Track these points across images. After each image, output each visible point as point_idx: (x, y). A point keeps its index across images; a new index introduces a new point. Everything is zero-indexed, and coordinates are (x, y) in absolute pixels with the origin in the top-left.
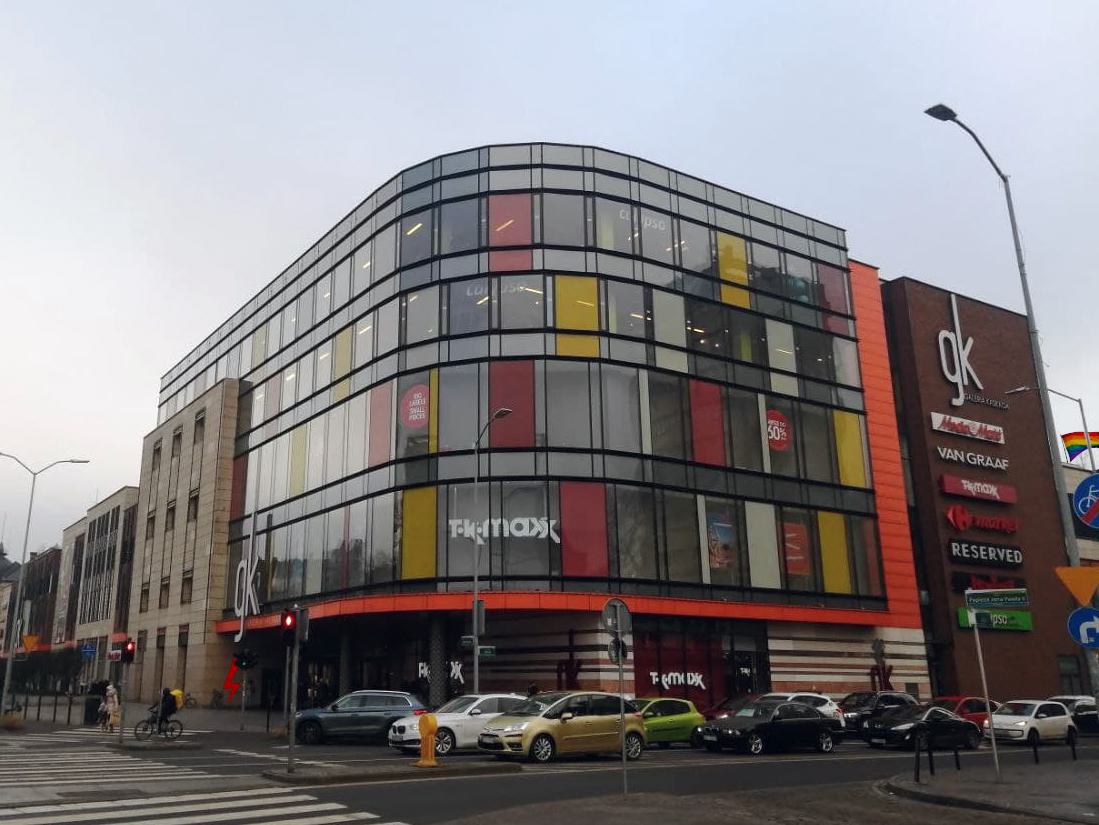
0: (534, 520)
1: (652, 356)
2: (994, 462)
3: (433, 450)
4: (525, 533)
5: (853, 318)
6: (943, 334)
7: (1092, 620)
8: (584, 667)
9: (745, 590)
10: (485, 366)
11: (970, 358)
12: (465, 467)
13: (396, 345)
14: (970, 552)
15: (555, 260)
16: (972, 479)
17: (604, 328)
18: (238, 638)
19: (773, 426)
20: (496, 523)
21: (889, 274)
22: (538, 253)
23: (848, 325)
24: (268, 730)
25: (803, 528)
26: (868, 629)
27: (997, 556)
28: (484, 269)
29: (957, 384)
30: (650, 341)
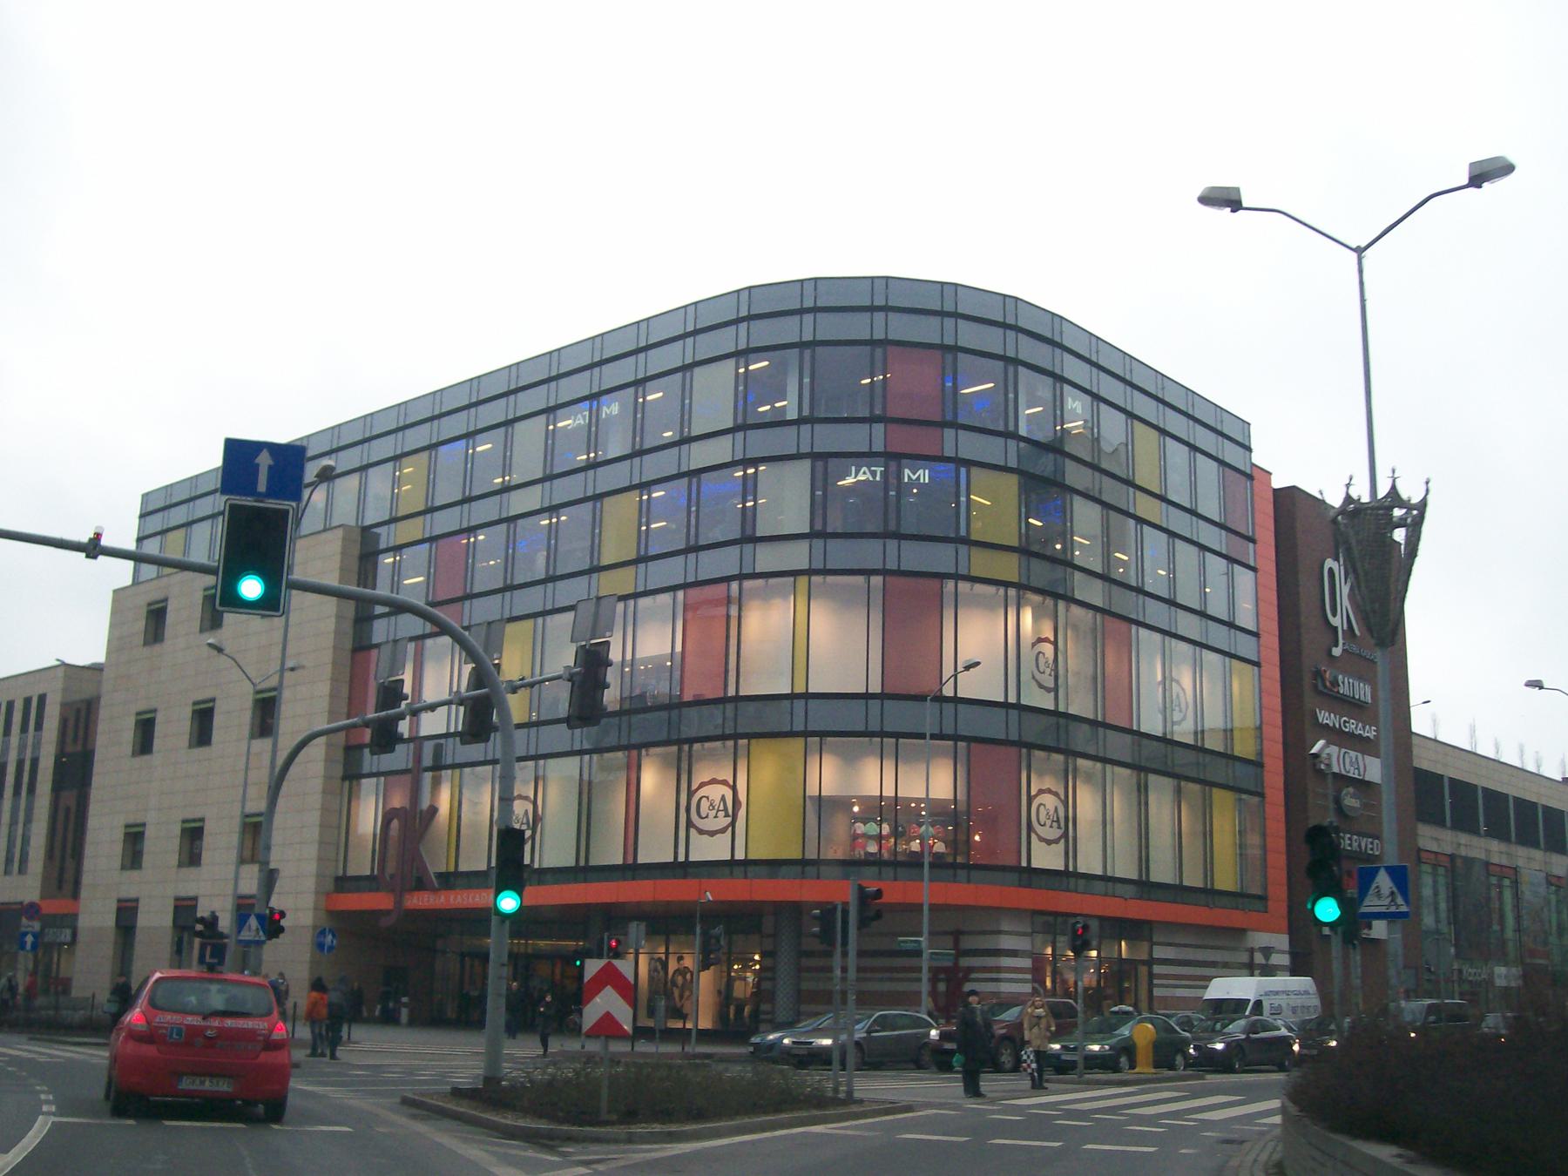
5: (1252, 540)
10: (877, 580)
13: (322, 527)
21: (1278, 482)
22: (949, 433)
23: (1248, 547)
24: (633, 1049)
26: (1240, 932)
27: (1360, 846)
28: (878, 447)
29: (1336, 628)
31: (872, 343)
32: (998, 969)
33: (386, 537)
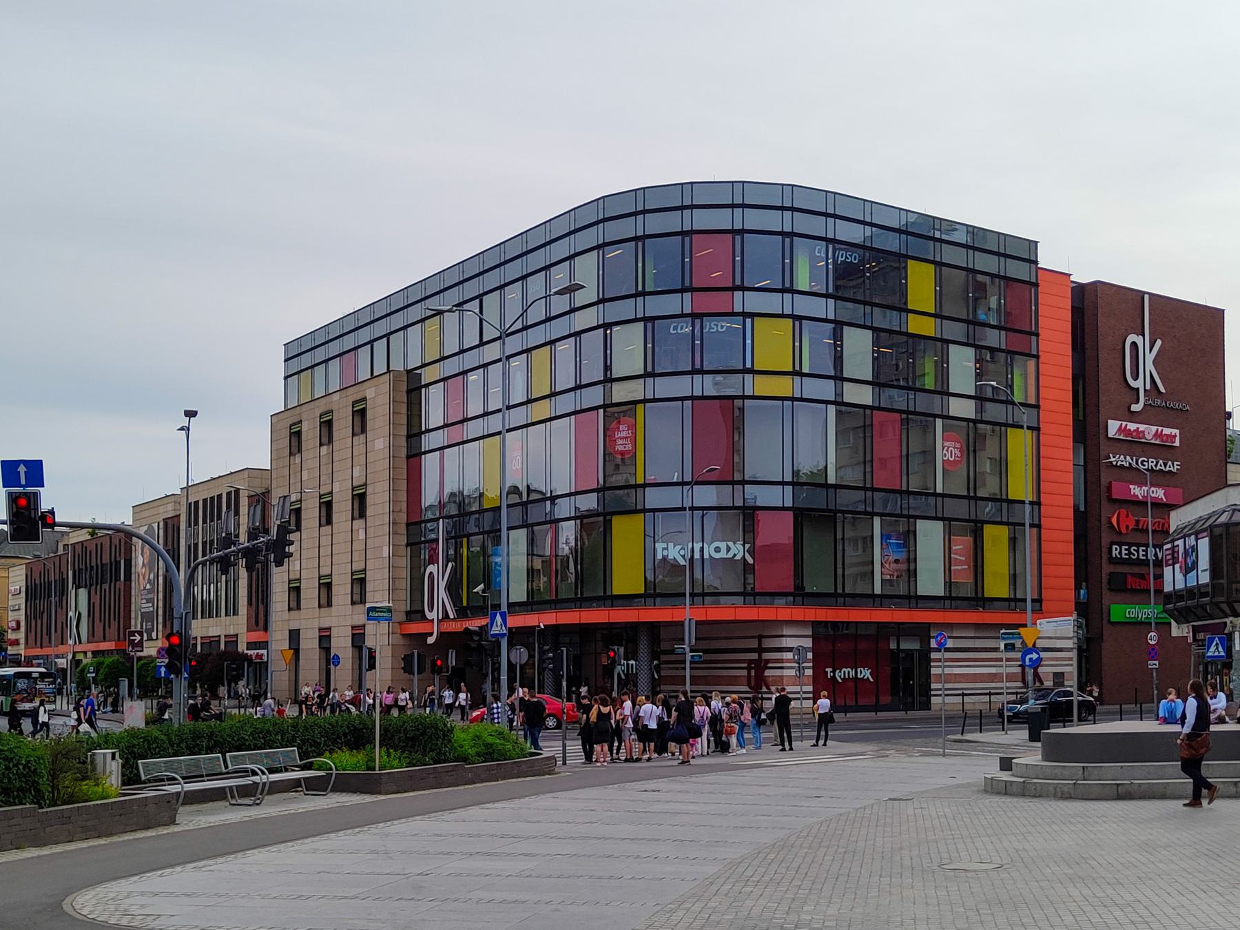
0: (730, 544)
1: (839, 393)
2: (1165, 465)
3: (640, 481)
4: (723, 555)
6: (1132, 338)
7: (1032, 653)
8: (770, 665)
9: (914, 600)
10: (688, 403)
11: (1154, 362)
12: (671, 497)
14: (1130, 553)
15: (754, 302)
16: (1141, 484)
17: (797, 368)
18: (431, 640)
19: (949, 447)
20: (697, 546)
21: (1082, 276)
22: (738, 294)
25: (969, 539)
28: (687, 310)
29: (1138, 389)
30: (839, 378)
31: (682, 233)
32: (782, 661)
33: (428, 375)
